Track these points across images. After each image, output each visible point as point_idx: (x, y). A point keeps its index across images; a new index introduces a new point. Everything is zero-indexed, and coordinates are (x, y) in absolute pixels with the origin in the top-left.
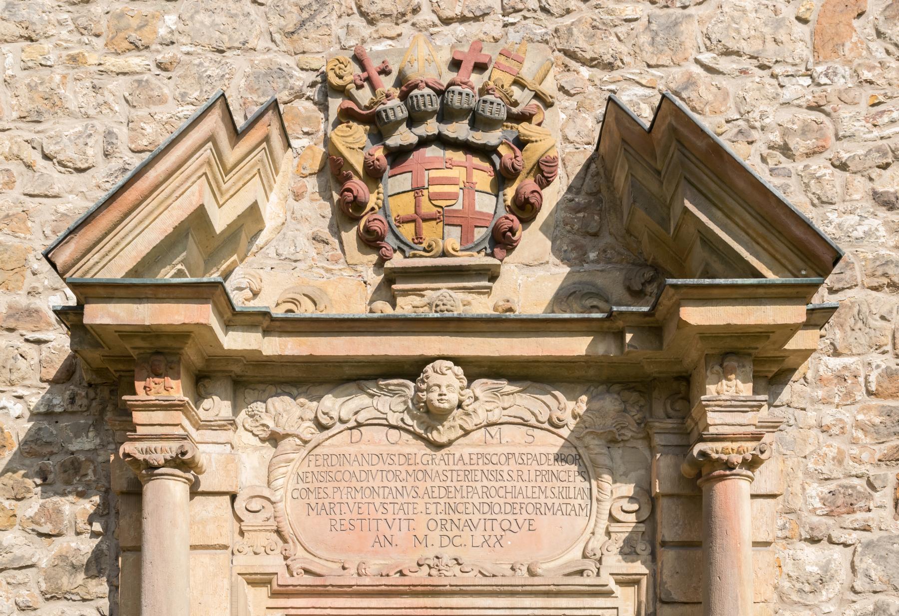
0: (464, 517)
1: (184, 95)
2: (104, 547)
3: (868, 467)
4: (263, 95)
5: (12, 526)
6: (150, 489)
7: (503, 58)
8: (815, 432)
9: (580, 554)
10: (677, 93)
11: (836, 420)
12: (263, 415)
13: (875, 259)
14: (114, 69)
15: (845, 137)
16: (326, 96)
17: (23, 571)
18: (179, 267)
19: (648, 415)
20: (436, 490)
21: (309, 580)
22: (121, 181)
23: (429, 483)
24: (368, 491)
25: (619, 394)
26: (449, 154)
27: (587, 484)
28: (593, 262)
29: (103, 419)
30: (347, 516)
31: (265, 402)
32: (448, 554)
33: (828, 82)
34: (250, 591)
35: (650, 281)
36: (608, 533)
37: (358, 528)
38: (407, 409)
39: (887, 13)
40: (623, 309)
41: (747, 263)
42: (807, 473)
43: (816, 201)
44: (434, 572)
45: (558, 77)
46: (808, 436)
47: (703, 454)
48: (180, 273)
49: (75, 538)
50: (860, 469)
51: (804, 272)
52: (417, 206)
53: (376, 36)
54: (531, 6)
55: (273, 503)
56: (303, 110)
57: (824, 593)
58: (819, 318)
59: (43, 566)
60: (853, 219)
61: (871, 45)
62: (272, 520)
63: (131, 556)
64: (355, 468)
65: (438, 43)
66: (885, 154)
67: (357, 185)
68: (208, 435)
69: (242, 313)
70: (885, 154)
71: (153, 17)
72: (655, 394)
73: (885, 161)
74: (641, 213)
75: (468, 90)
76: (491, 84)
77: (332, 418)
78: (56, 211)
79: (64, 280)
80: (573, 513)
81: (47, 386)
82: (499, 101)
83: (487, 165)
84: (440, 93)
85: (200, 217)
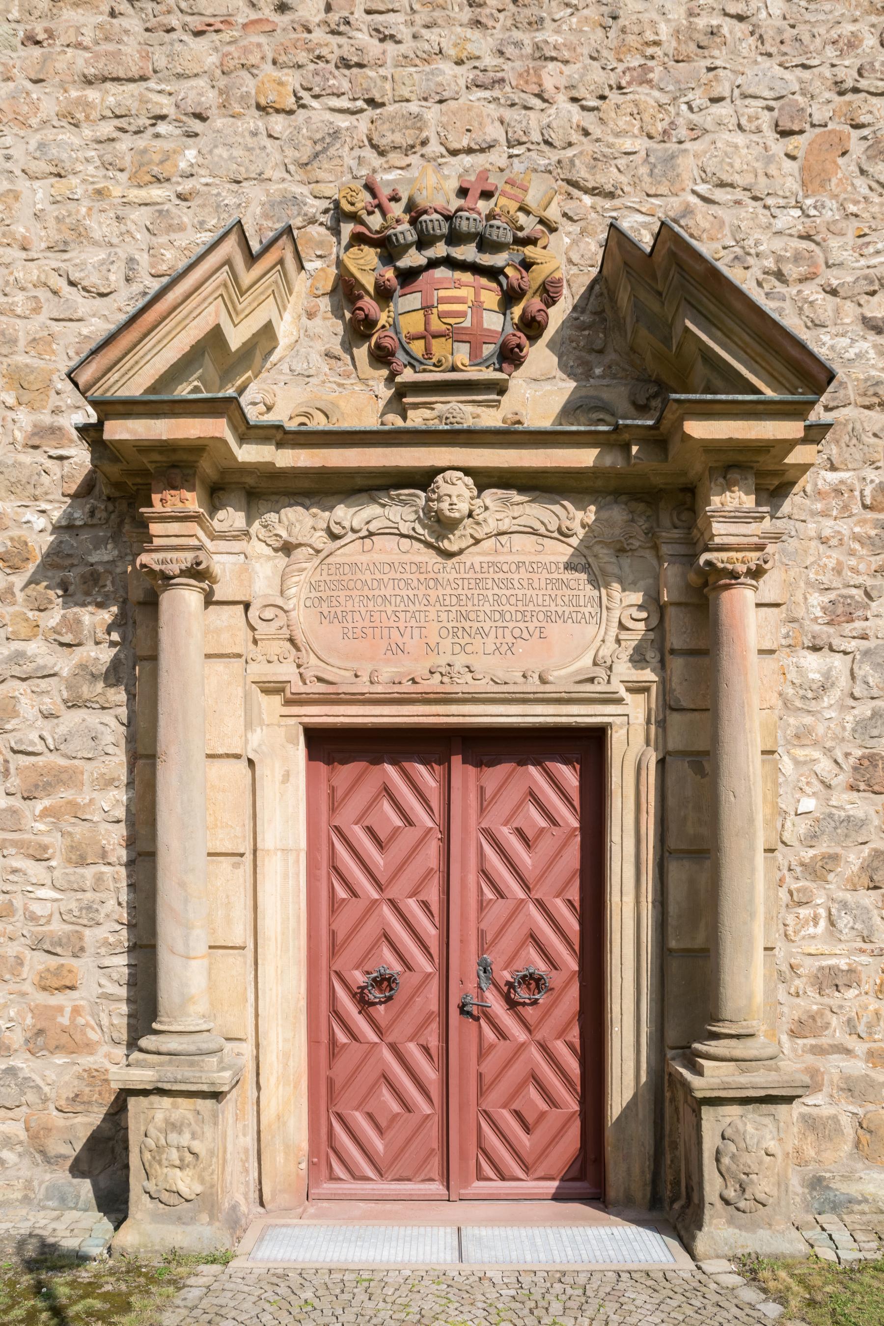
0: (476, 625)
1: (202, 223)
2: (122, 656)
3: (865, 577)
4: (278, 221)
5: (35, 636)
6: (166, 599)
7: (508, 186)
8: (814, 544)
9: (590, 662)
10: (676, 221)
11: (835, 532)
12: (276, 525)
13: (866, 380)
14: (136, 200)
15: (834, 265)
16: (338, 221)
17: (46, 679)
18: (196, 383)
19: (655, 525)
20: (447, 598)
21: (322, 688)
22: (140, 304)
23: (441, 592)
24: (380, 599)
25: (626, 504)
26: (458, 275)
27: (596, 593)
28: (599, 377)
29: (120, 531)
30: (360, 624)
31: (278, 512)
32: (460, 661)
33: (817, 213)
34: (264, 699)
35: (655, 396)
36: (618, 641)
37: (370, 636)
38: (419, 518)
39: (869, 153)
40: (629, 422)
41: (746, 380)
42: (808, 583)
43: (810, 324)
44: (446, 679)
45: (562, 204)
46: (809, 548)
47: (709, 563)
48: (196, 390)
49: (95, 647)
50: (859, 580)
51: (800, 390)
52: (427, 323)
53: (386, 166)
54: (535, 139)
55: (286, 612)
56: (315, 235)
57: (826, 699)
58: (816, 434)
59: (65, 675)
60: (844, 342)
61: (855, 181)
62: (285, 628)
63: (147, 665)
64: (367, 576)
65: (446, 173)
66: (872, 282)
67: (369, 304)
68: (222, 545)
69: (256, 427)
70: (872, 282)
71: (175, 152)
72: (662, 504)
73: (872, 288)
74: (644, 332)
75: (475, 216)
76: (497, 210)
77: (344, 528)
78: (80, 334)
79: (86, 398)
80: (583, 621)
81: (68, 500)
82: (505, 226)
83: (494, 285)
84: (448, 218)
85: (216, 335)
